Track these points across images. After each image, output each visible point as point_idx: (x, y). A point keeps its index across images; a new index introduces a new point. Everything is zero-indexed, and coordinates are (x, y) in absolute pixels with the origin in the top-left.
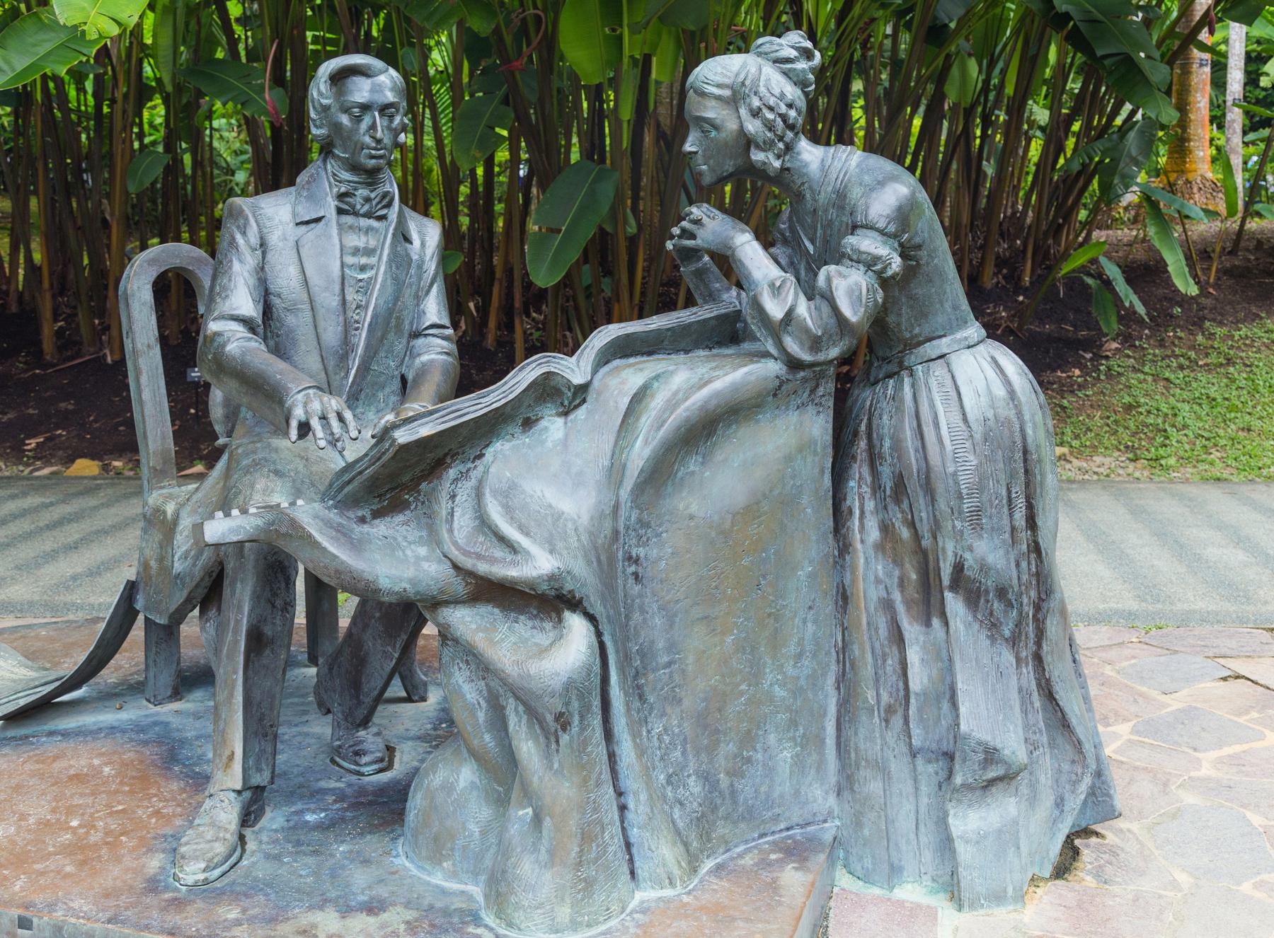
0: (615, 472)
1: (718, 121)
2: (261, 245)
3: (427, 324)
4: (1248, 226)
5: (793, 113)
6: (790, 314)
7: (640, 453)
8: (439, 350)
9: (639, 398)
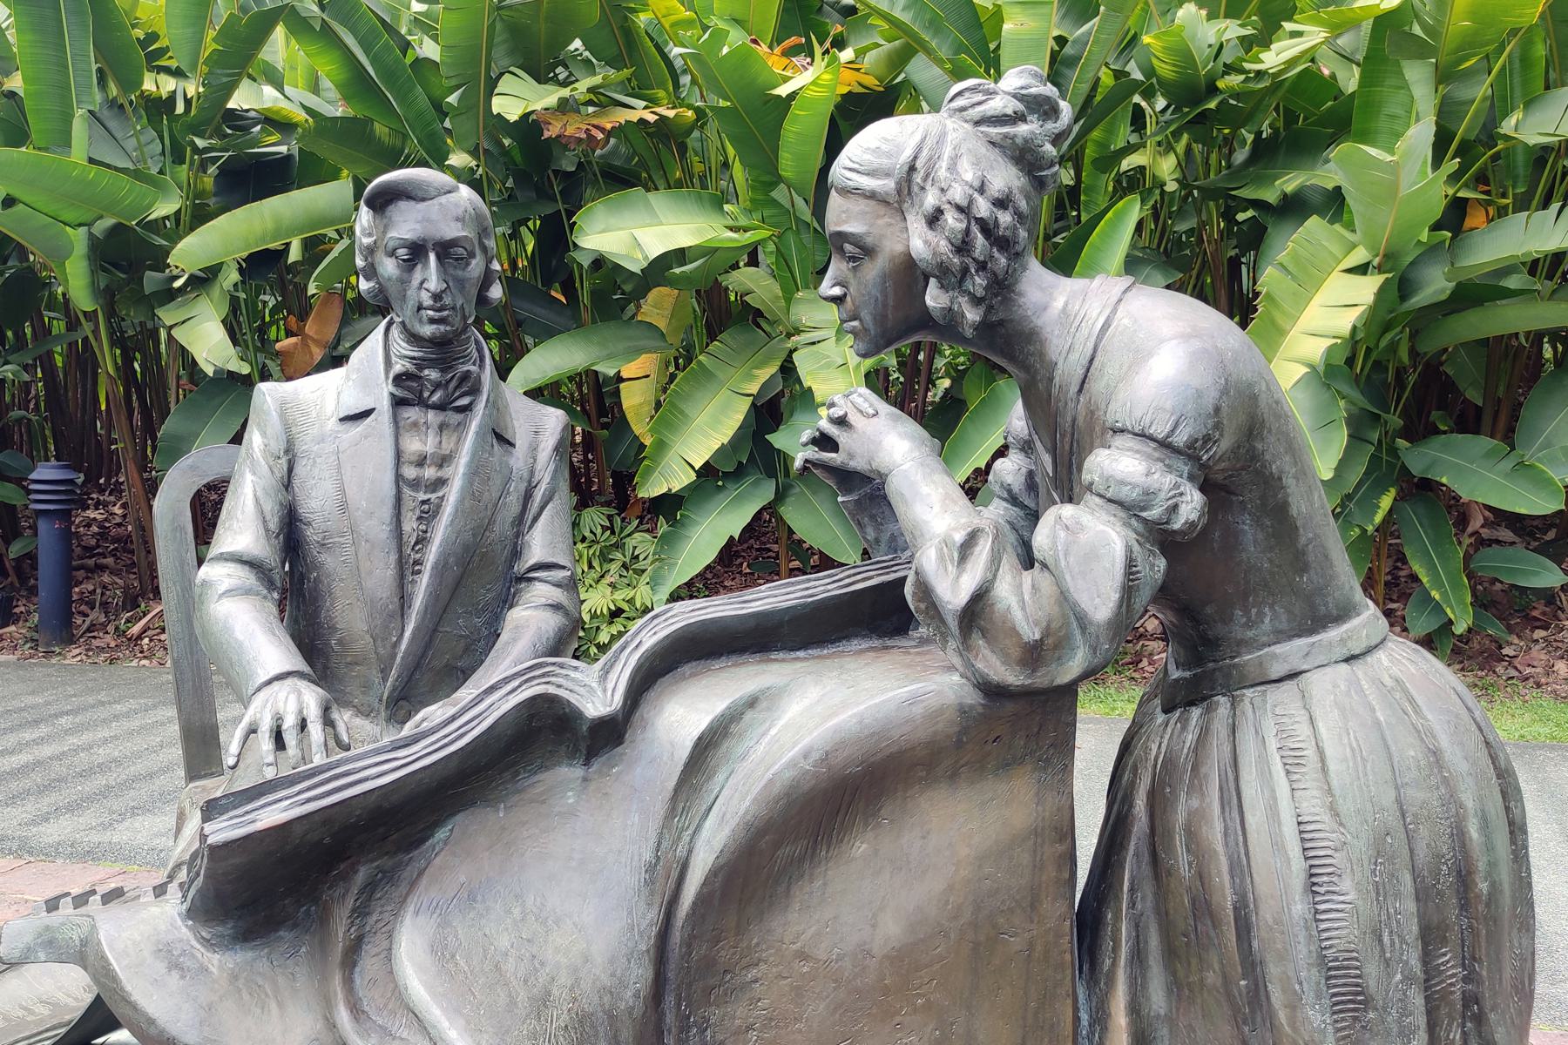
0: (666, 874)
1: (869, 240)
2: (287, 452)
3: (531, 562)
4: (1508, 126)
5: (1005, 218)
6: (980, 599)
7: (711, 843)
8: (543, 601)
9: (707, 750)
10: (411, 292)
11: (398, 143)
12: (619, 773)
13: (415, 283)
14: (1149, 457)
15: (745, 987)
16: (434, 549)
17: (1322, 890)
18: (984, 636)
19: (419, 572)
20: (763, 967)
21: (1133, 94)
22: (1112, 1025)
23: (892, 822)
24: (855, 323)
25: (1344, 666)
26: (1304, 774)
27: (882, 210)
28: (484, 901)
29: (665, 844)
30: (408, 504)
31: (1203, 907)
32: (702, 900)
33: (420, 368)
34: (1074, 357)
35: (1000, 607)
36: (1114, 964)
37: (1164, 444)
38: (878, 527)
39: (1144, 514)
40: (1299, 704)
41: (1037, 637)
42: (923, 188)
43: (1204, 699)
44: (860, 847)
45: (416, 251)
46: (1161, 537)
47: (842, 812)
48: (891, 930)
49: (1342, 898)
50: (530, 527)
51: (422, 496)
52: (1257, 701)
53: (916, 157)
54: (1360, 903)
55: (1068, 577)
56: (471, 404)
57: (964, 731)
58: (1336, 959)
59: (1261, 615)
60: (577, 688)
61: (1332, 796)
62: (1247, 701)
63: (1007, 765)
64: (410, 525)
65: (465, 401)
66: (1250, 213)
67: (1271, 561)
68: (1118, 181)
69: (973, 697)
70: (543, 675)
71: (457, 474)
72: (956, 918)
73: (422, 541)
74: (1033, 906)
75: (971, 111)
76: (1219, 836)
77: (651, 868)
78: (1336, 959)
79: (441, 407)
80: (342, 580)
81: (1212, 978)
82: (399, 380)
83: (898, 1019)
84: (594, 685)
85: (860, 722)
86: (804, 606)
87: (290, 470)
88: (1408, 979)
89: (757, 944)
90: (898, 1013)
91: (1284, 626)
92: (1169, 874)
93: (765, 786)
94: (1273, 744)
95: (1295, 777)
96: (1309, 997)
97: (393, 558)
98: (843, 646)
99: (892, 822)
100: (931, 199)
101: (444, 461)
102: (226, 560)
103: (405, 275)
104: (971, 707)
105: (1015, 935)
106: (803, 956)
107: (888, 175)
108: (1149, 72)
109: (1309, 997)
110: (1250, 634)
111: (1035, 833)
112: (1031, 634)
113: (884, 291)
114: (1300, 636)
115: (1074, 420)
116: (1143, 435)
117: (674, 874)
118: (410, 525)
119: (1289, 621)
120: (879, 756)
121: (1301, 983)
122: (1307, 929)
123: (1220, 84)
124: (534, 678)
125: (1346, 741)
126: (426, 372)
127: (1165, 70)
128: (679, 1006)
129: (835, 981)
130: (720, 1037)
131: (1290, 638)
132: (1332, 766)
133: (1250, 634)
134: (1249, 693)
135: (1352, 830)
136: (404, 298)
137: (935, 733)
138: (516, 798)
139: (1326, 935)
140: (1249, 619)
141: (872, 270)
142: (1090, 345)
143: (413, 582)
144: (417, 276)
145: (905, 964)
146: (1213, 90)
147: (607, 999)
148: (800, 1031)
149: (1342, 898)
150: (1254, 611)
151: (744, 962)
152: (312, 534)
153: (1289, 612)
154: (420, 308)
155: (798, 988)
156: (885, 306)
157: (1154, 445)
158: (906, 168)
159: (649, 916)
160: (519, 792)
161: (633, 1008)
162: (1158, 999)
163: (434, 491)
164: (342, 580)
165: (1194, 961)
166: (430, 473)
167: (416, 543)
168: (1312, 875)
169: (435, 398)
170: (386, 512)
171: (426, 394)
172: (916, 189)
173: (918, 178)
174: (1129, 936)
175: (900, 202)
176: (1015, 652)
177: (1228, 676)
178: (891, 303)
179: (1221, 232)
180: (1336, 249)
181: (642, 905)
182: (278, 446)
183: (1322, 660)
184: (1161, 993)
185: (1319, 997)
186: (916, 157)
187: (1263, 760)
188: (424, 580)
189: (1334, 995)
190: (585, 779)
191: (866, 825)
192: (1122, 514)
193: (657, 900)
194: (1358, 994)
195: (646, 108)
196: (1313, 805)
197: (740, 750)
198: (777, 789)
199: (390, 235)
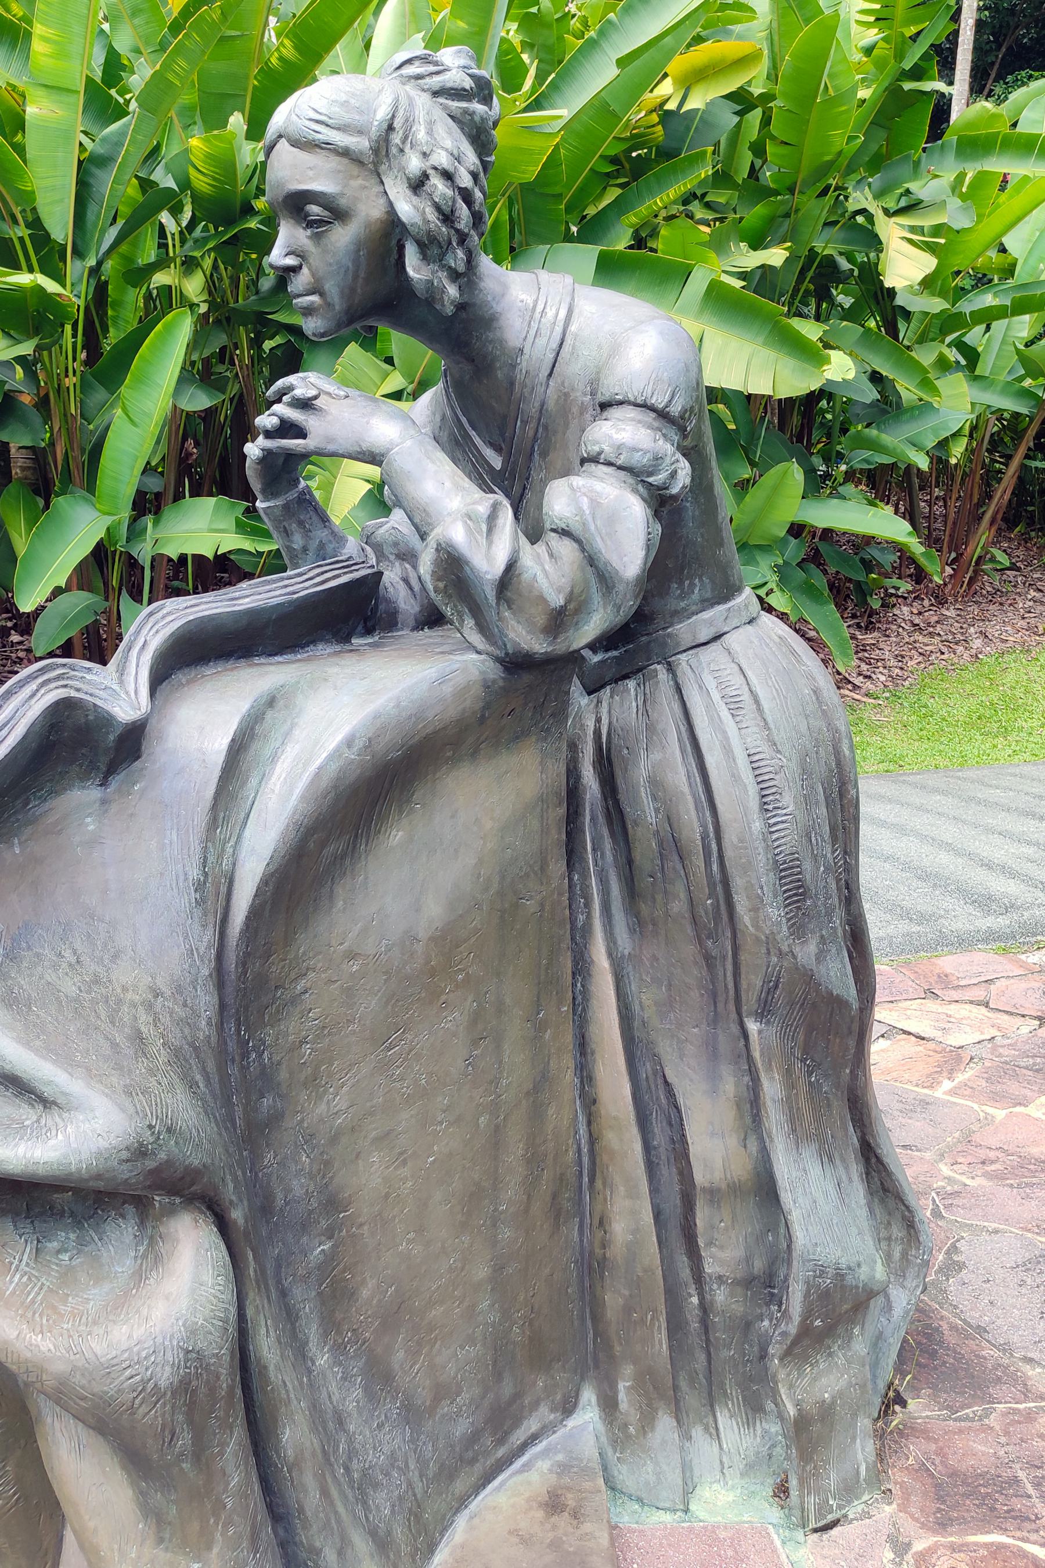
0: (214, 889)
1: (343, 202)
12: (143, 791)
14: (650, 427)
15: (295, 1000)
17: (770, 807)
18: (510, 608)
20: (311, 975)
21: (159, 210)
22: (594, 971)
23: (424, 806)
24: (314, 298)
25: (748, 627)
26: (744, 715)
27: (355, 170)
28: (29, 948)
29: (211, 859)
31: (672, 845)
32: (255, 913)
34: (541, 342)
35: (526, 577)
36: (589, 916)
37: (662, 414)
38: (307, 533)
39: (650, 480)
40: (728, 659)
41: (562, 603)
42: (402, 151)
43: (640, 670)
44: (396, 836)
46: (661, 503)
47: (381, 802)
48: (434, 912)
49: (784, 811)
52: (693, 662)
53: (393, 116)
54: (797, 812)
55: (598, 539)
57: (487, 706)
58: (785, 862)
59: (692, 585)
60: (97, 692)
61: (769, 729)
62: (684, 664)
63: (518, 737)
66: (279, 340)
67: (702, 536)
68: (148, 297)
69: (494, 671)
70: (58, 678)
72: (486, 889)
74: (543, 869)
75: (428, 80)
76: (684, 779)
77: (200, 887)
78: (785, 862)
81: (679, 906)
83: (444, 998)
84: (116, 687)
85: (398, 706)
86: (290, 602)
88: (827, 869)
89: (304, 953)
90: (443, 992)
91: (709, 595)
92: (636, 823)
93: (312, 782)
94: (716, 696)
95: (738, 719)
96: (768, 898)
98: (311, 651)
99: (424, 806)
100: (414, 164)
104: (494, 681)
105: (531, 898)
106: (352, 955)
107: (360, 132)
108: (185, 184)
109: (768, 898)
110: (682, 604)
111: (542, 799)
112: (557, 600)
113: (356, 261)
114: (719, 604)
115: (542, 405)
116: (644, 406)
117: (223, 889)
119: (713, 590)
120: (417, 738)
121: (762, 888)
122: (764, 841)
124: (49, 681)
125: (770, 684)
127: (201, 183)
128: (239, 1031)
129: (385, 973)
130: (276, 1058)
131: (712, 605)
132: (766, 705)
133: (682, 604)
134: (683, 657)
135: (787, 754)
137: (464, 709)
138: (28, 831)
139: (776, 844)
140: (683, 592)
141: (343, 237)
142: (559, 329)
145: (447, 941)
146: (248, 210)
147: (187, 1031)
148: (354, 1032)
149: (784, 811)
150: (687, 583)
151: (293, 975)
153: (713, 582)
155: (349, 988)
156: (356, 277)
157: (653, 415)
158: (385, 126)
159: (205, 939)
160: (30, 822)
161: (209, 1037)
162: (625, 942)
165: (659, 897)
168: (763, 796)
172: (394, 150)
173: (396, 139)
174: (598, 889)
175: (377, 164)
176: (541, 620)
177: (664, 645)
178: (362, 275)
179: (252, 358)
180: (375, 376)
181: (197, 926)
183: (735, 622)
184: (625, 936)
185: (775, 896)
186: (393, 116)
187: (710, 706)
189: (785, 892)
190: (104, 802)
191: (401, 812)
192: (631, 480)
193: (211, 919)
194: (799, 887)
196: (755, 739)
197: (267, 752)
198: (325, 783)
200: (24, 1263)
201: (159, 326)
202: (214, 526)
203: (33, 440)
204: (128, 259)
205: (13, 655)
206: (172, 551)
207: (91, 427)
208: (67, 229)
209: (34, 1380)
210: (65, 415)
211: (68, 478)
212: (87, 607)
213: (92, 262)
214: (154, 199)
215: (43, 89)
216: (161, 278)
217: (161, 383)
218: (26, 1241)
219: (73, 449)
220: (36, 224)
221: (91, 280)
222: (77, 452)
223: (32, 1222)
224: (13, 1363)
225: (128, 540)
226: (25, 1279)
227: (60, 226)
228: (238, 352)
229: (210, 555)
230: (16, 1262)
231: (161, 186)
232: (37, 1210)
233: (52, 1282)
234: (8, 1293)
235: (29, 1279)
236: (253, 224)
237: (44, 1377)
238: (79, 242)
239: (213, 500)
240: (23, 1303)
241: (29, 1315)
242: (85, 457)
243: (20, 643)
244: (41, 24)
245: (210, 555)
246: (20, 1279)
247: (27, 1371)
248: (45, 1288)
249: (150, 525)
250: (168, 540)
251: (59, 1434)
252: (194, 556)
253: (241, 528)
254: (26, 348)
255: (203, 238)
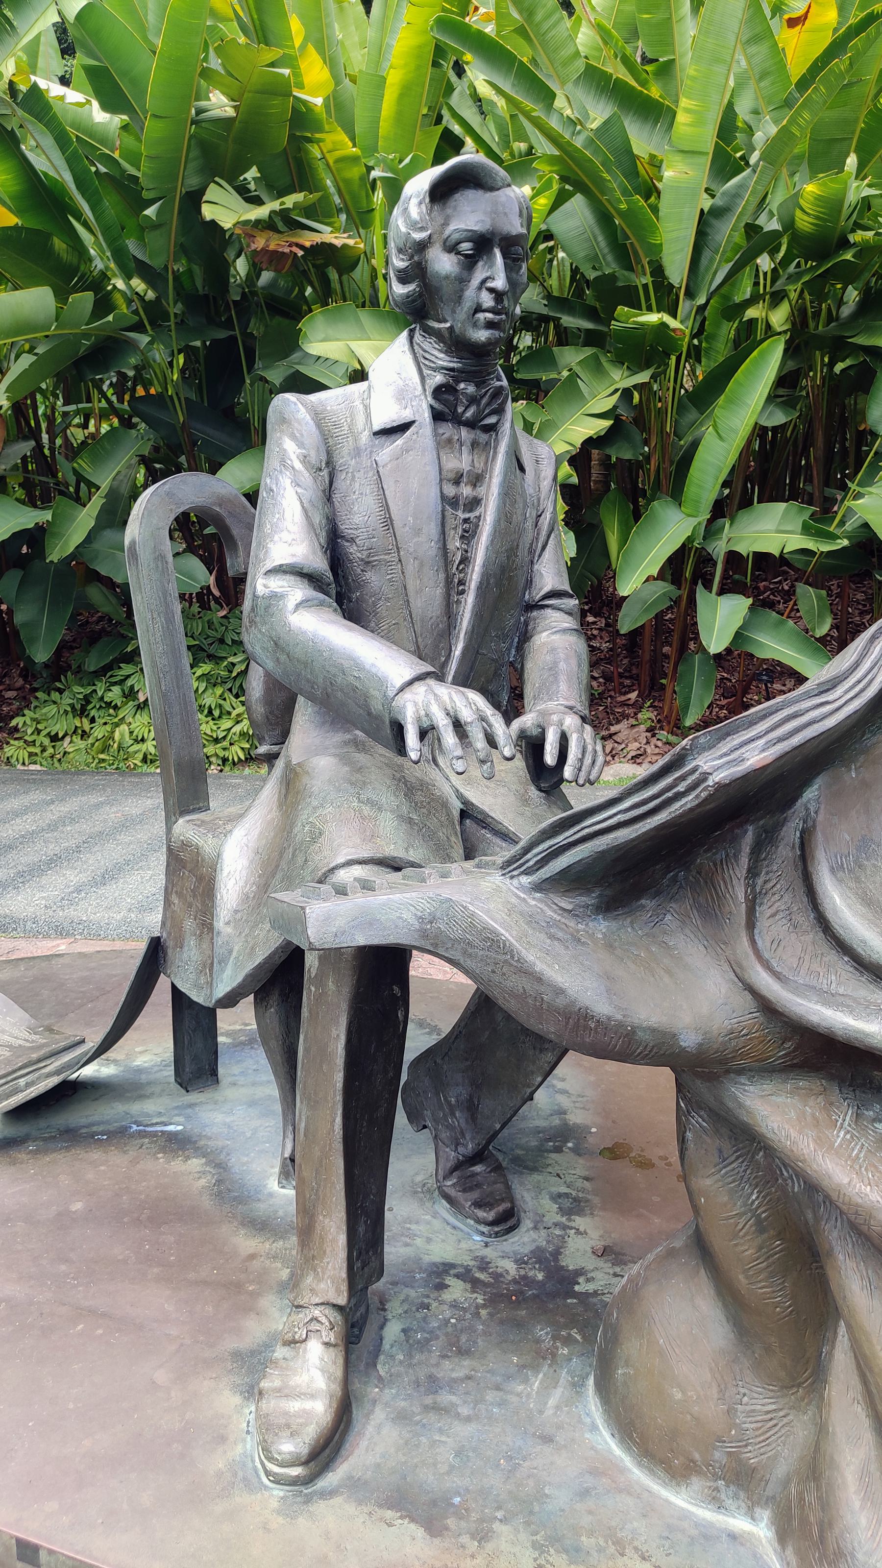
2: (328, 463)
3: (542, 593)
10: (470, 292)
11: (75, 261)
13: (475, 282)
16: (477, 568)
19: (463, 592)
30: (450, 522)
33: (458, 382)
45: (482, 244)
50: (540, 556)
51: (462, 515)
56: (497, 423)
64: (455, 543)
65: (492, 420)
71: (492, 494)
73: (465, 560)
79: (471, 424)
80: (388, 600)
82: (438, 392)
87: (331, 483)
97: (442, 576)
101: (477, 480)
102: (285, 572)
103: (465, 274)
118: (455, 543)
123: (852, 238)
126: (462, 386)
136: (459, 298)
143: (458, 602)
144: (479, 274)
146: (844, 243)
152: (354, 551)
154: (478, 309)
163: (471, 511)
164: (388, 600)
166: (466, 491)
167: (460, 563)
169: (469, 414)
170: (432, 529)
171: (460, 410)
182: (317, 457)
188: (470, 599)
195: (332, 232)
199: (452, 227)
200: (846, 1123)
201: (755, 353)
202: (782, 528)
203: (633, 455)
204: (727, 298)
205: (589, 633)
206: (743, 548)
207: (682, 442)
208: (683, 274)
209: (861, 1222)
210: (662, 432)
211: (657, 486)
212: (664, 594)
213: (701, 300)
214: (757, 240)
215: (680, 154)
216: (752, 313)
217: (749, 402)
218: (849, 1105)
219: (664, 462)
220: (658, 271)
221: (698, 317)
222: (667, 464)
223: (854, 1090)
224: (843, 1203)
225: (704, 538)
226: (848, 1136)
227: (677, 271)
228: (811, 374)
229: (777, 553)
230: (840, 1121)
231: (765, 230)
232: (858, 1082)
233: (870, 1145)
234: (836, 1144)
235: (852, 1137)
236: (848, 256)
237: (872, 1223)
238: (692, 284)
239: (783, 505)
240: (850, 1156)
241: (857, 1167)
242: (674, 467)
243: (594, 623)
244: (687, 98)
245: (777, 553)
246: (845, 1136)
247: (856, 1213)
248: (865, 1149)
249: (727, 526)
250: (741, 539)
251: (850, 1272)
252: (754, 553)
253: (806, 530)
254: (643, 377)
255: (796, 273)
